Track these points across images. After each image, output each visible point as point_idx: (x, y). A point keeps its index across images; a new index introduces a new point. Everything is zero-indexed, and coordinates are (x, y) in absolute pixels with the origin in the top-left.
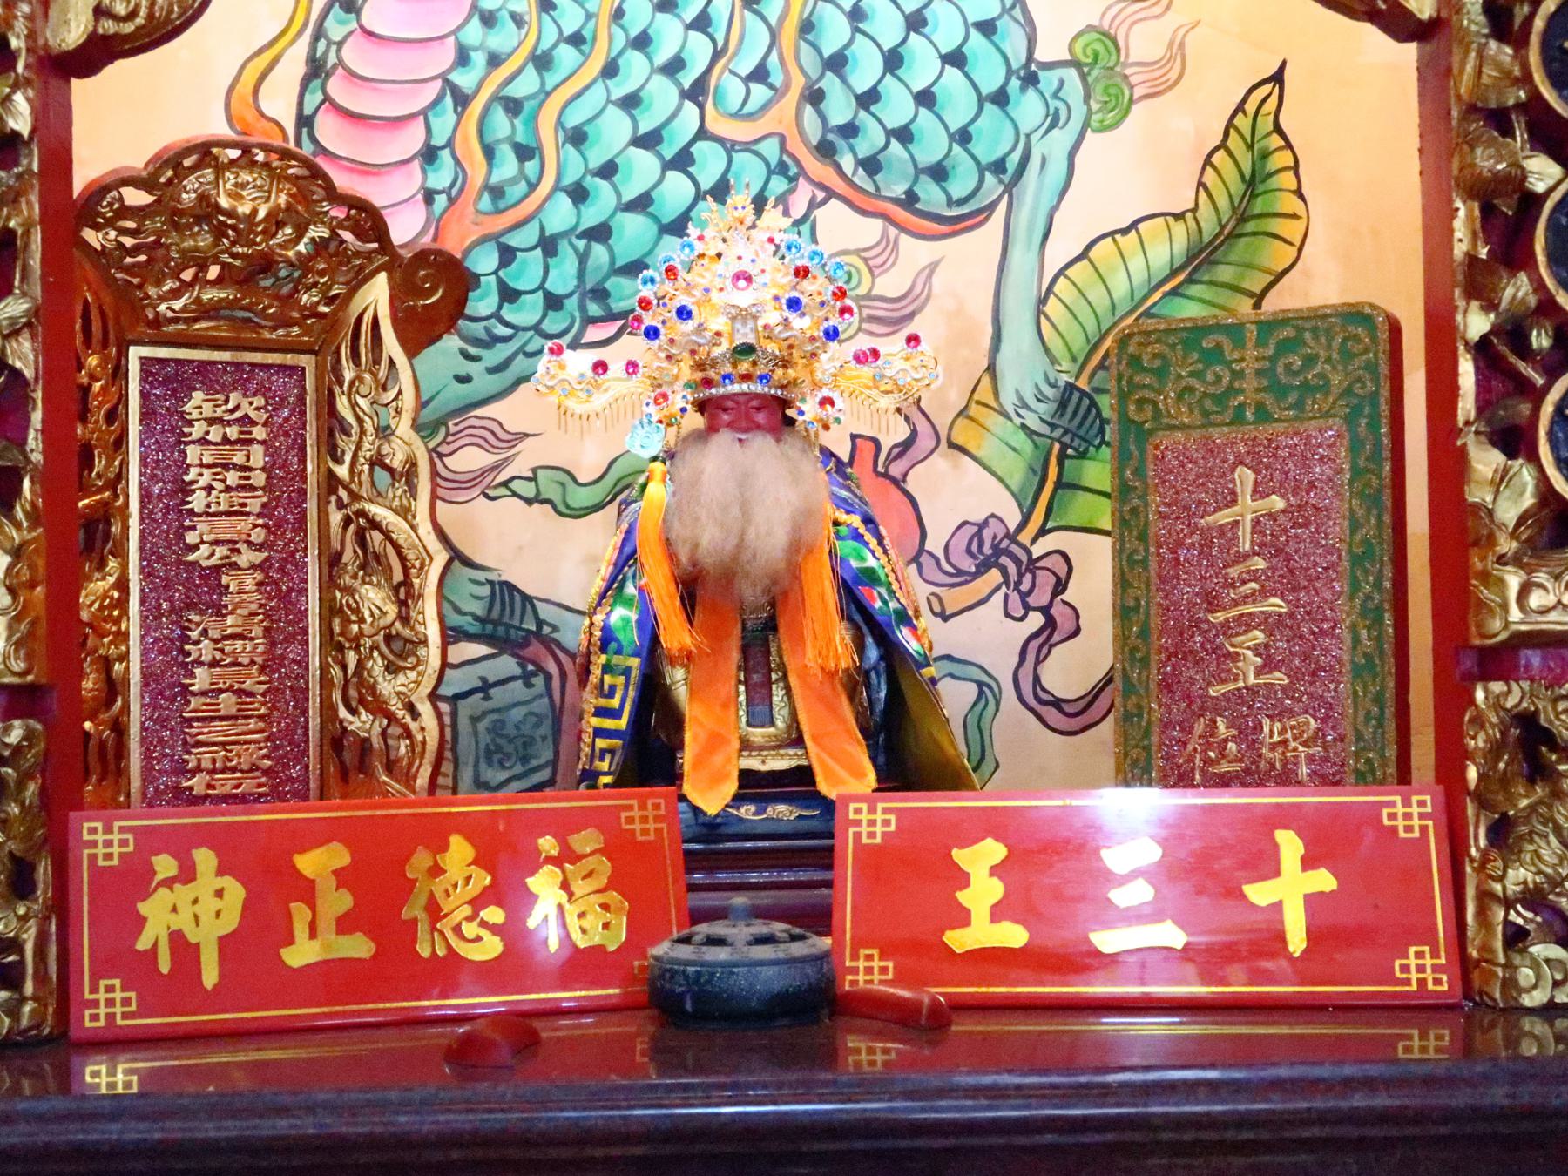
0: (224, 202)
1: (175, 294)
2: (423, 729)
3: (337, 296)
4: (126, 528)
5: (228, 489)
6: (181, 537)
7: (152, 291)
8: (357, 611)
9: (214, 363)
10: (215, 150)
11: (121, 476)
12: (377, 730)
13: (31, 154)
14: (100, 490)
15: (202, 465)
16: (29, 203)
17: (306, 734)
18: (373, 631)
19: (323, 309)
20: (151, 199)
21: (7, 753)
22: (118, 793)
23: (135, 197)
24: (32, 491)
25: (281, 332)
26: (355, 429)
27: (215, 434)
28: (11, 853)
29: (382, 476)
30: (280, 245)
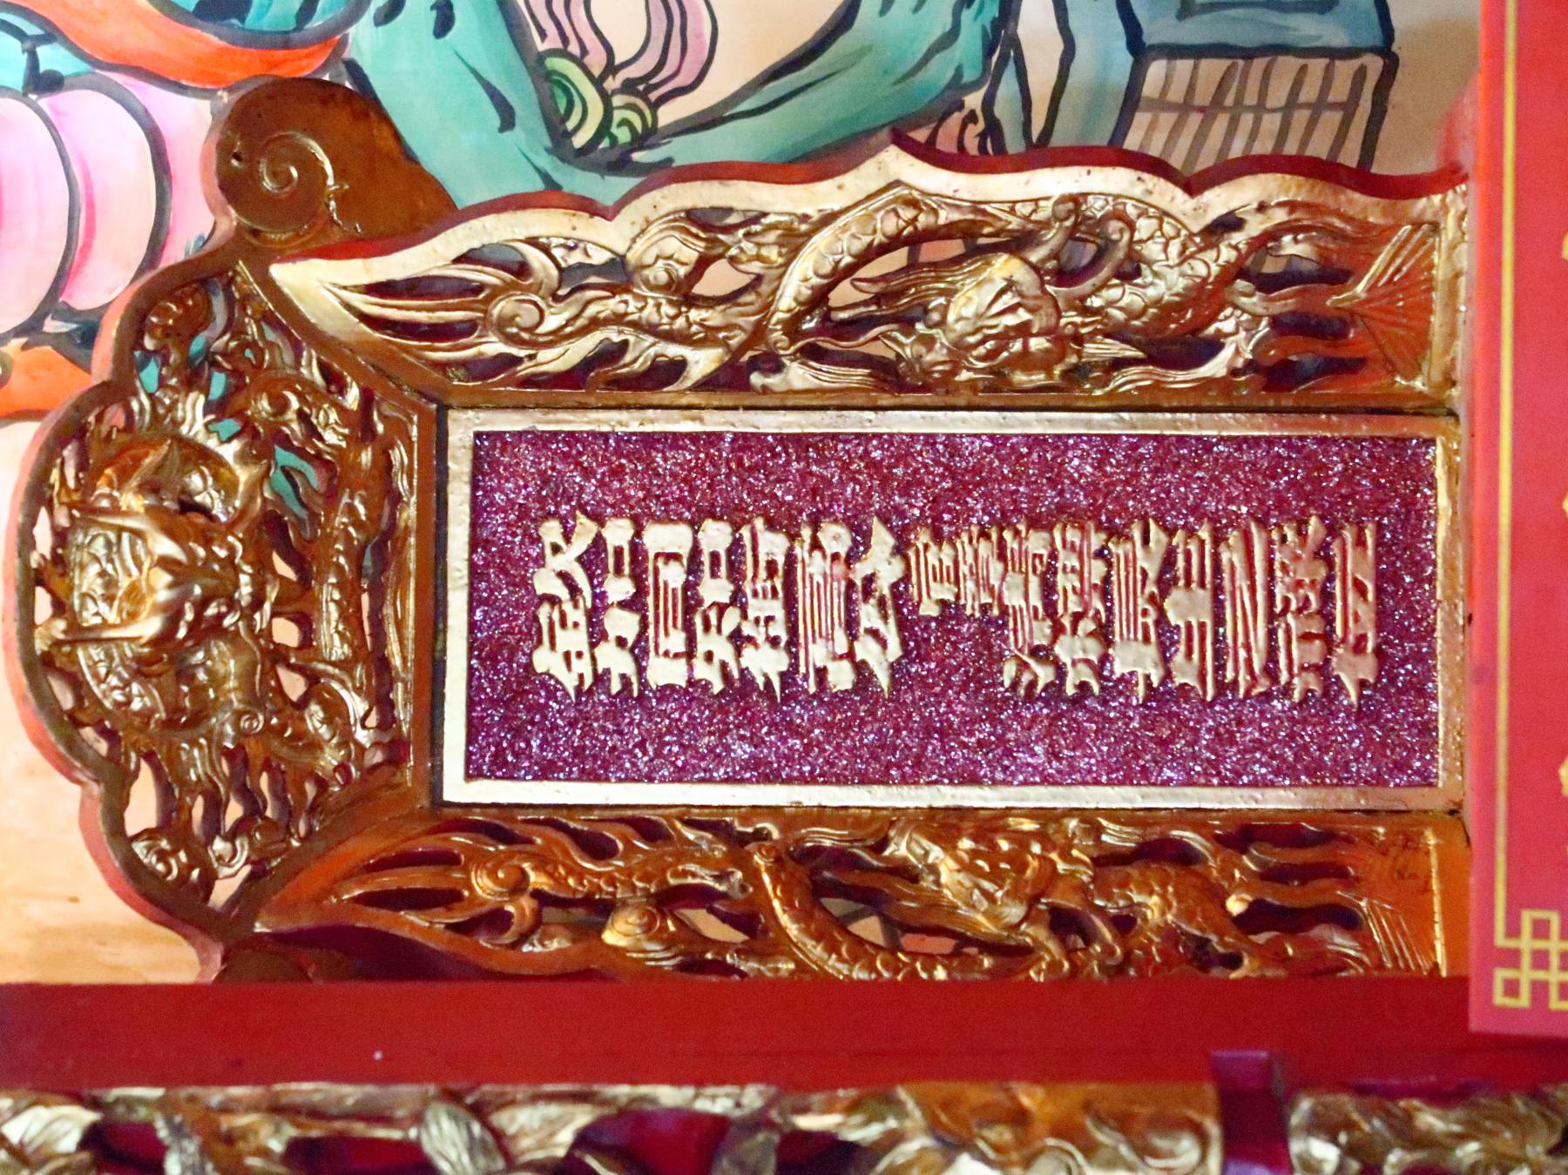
0: (149, 626)
1: (335, 711)
2: (1262, 208)
3: (325, 369)
4: (821, 815)
5: (737, 598)
6: (842, 698)
7: (330, 758)
8: (1005, 337)
9: (473, 626)
10: (40, 646)
11: (713, 823)
12: (1254, 302)
13: (130, 1103)
14: (753, 875)
15: (690, 654)
16: (227, 1109)
17: (1256, 441)
18: (1048, 309)
19: (352, 398)
20: (146, 771)
21: (1355, 1166)
22: (1369, 838)
23: (142, 810)
24: (828, 1109)
25: (402, 484)
26: (613, 335)
27: (622, 624)
28: (1554, 1151)
29: (718, 280)
30: (226, 502)
